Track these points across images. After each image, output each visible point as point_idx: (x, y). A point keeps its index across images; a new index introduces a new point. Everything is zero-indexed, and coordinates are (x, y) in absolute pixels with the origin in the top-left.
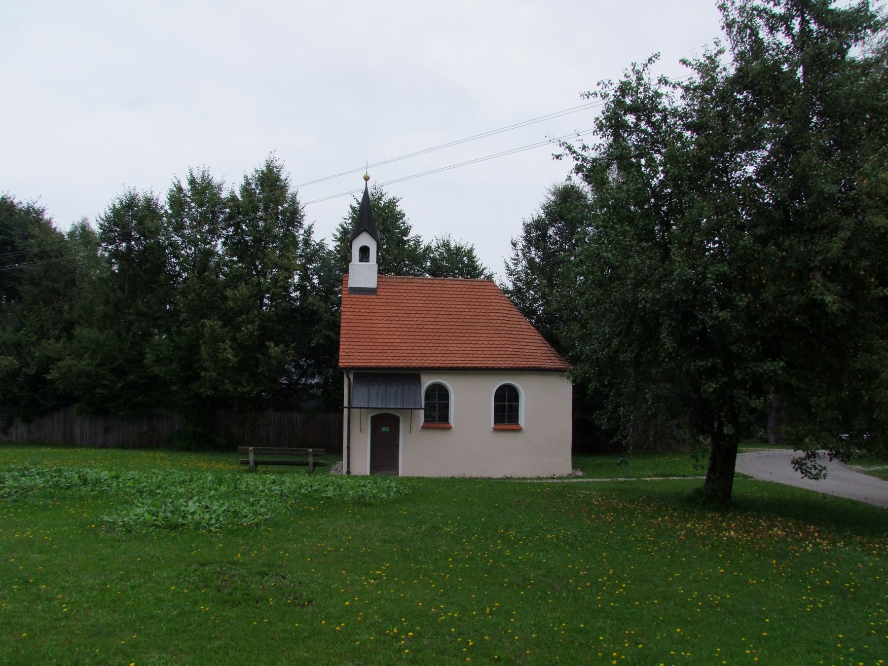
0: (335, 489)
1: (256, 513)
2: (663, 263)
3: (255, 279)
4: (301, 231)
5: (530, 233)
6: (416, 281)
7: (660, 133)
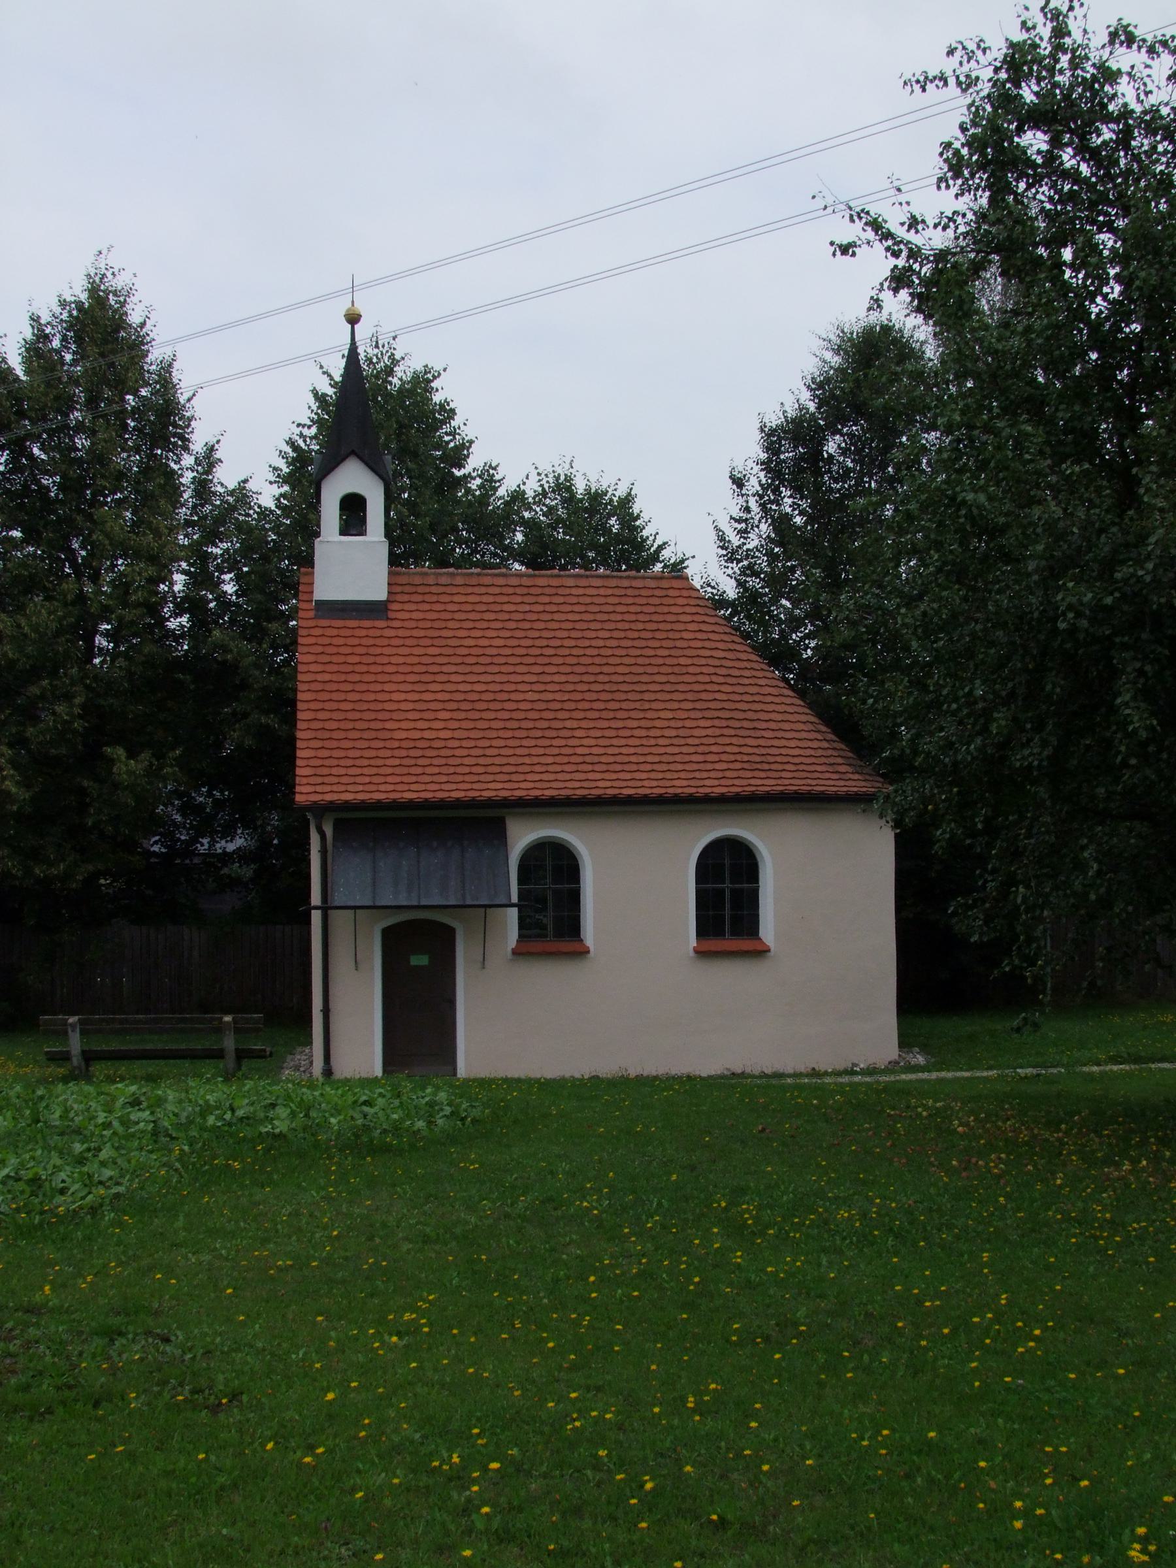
0: (293, 1114)
1: (89, 1182)
2: (1121, 516)
3: (70, 586)
4: (188, 460)
5: (777, 452)
6: (487, 580)
7: (1112, 179)
